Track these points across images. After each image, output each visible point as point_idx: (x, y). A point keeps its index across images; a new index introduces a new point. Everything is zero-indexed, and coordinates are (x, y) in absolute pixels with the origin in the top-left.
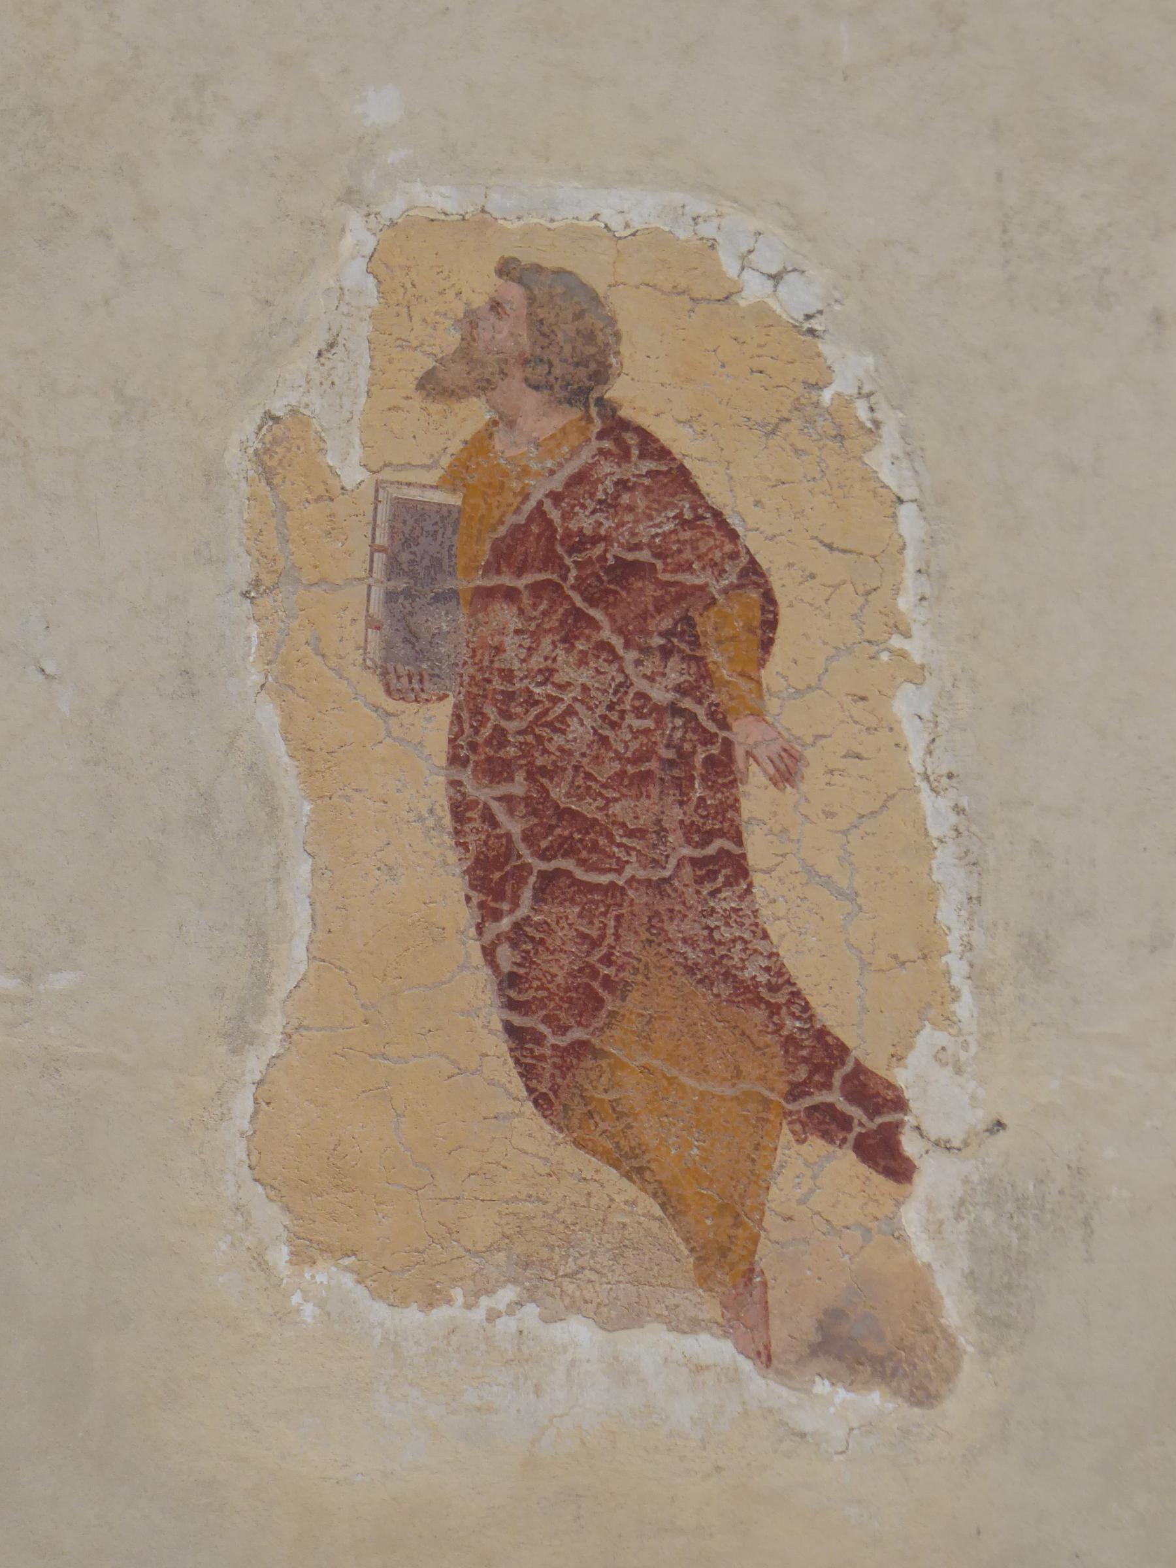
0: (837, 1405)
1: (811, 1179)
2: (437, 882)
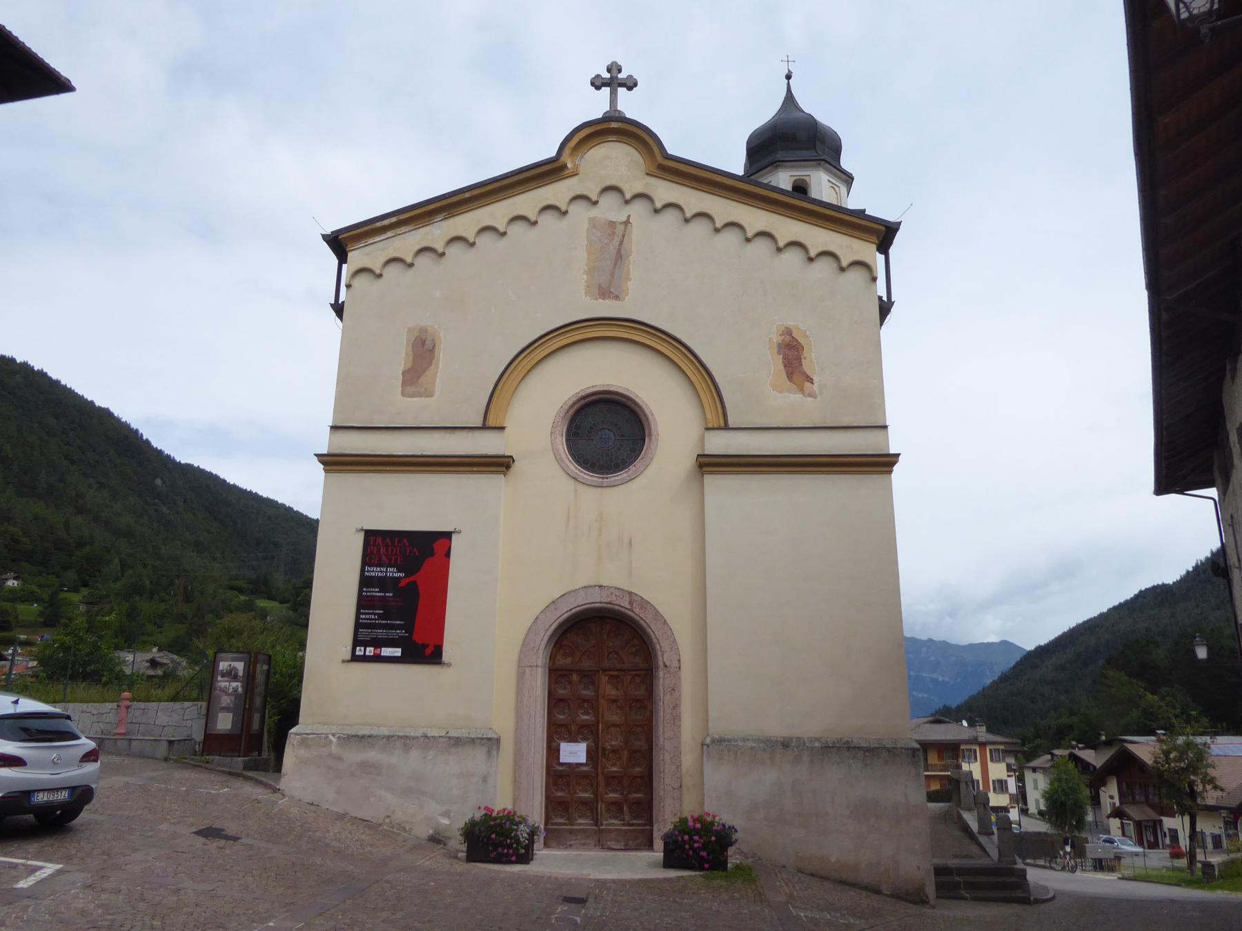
0: (809, 399)
1: (807, 385)
2: (782, 367)
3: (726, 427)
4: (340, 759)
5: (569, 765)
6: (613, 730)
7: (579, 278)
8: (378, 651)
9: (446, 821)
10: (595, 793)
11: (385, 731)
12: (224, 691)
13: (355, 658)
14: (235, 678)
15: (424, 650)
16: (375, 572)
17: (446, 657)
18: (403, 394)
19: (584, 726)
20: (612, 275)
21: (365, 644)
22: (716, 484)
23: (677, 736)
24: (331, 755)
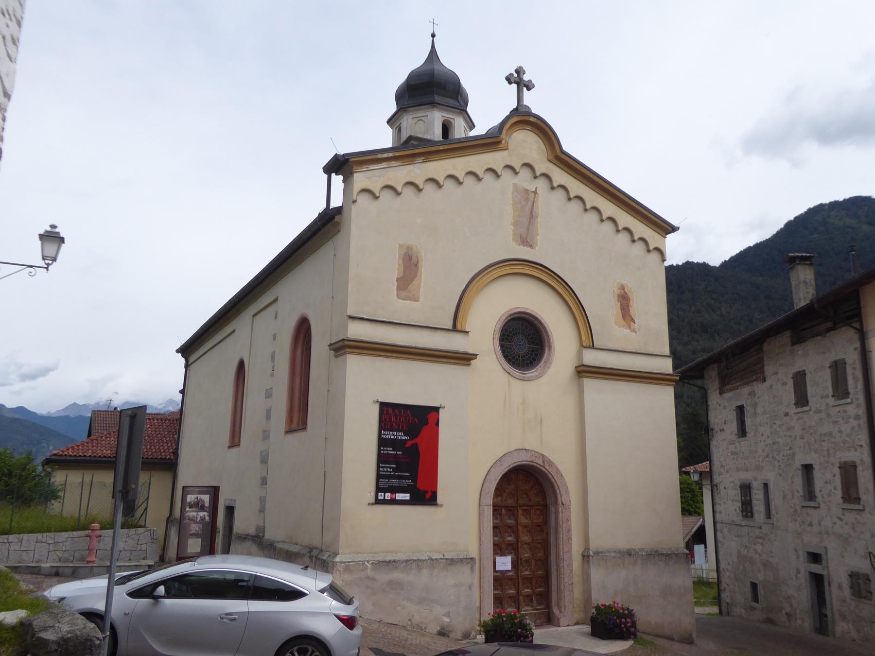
1: (632, 324)
3: (593, 347)
4: (374, 579)
5: (502, 572)
6: (525, 546)
7: (508, 229)
8: (393, 496)
9: (447, 620)
10: (518, 590)
11: (401, 556)
12: (193, 520)
13: (378, 502)
14: (202, 508)
15: (425, 495)
16: (388, 435)
17: (439, 501)
18: (398, 297)
19: (510, 544)
20: (528, 229)
21: (385, 491)
22: (590, 384)
23: (570, 550)
24: (368, 578)
